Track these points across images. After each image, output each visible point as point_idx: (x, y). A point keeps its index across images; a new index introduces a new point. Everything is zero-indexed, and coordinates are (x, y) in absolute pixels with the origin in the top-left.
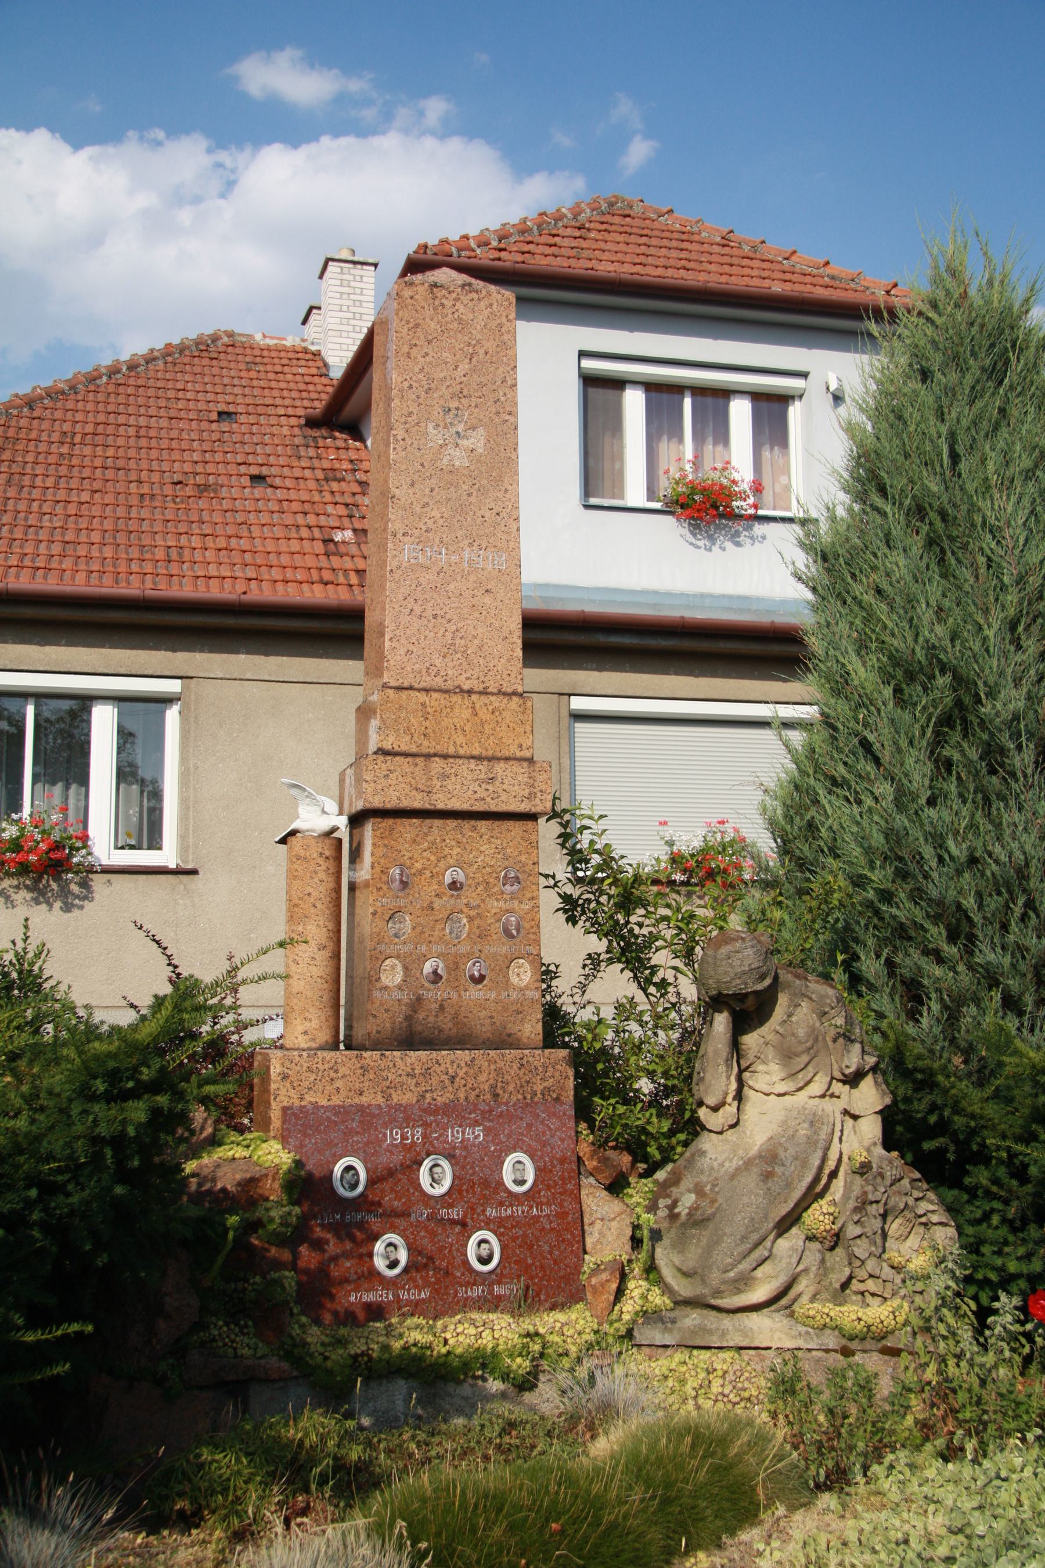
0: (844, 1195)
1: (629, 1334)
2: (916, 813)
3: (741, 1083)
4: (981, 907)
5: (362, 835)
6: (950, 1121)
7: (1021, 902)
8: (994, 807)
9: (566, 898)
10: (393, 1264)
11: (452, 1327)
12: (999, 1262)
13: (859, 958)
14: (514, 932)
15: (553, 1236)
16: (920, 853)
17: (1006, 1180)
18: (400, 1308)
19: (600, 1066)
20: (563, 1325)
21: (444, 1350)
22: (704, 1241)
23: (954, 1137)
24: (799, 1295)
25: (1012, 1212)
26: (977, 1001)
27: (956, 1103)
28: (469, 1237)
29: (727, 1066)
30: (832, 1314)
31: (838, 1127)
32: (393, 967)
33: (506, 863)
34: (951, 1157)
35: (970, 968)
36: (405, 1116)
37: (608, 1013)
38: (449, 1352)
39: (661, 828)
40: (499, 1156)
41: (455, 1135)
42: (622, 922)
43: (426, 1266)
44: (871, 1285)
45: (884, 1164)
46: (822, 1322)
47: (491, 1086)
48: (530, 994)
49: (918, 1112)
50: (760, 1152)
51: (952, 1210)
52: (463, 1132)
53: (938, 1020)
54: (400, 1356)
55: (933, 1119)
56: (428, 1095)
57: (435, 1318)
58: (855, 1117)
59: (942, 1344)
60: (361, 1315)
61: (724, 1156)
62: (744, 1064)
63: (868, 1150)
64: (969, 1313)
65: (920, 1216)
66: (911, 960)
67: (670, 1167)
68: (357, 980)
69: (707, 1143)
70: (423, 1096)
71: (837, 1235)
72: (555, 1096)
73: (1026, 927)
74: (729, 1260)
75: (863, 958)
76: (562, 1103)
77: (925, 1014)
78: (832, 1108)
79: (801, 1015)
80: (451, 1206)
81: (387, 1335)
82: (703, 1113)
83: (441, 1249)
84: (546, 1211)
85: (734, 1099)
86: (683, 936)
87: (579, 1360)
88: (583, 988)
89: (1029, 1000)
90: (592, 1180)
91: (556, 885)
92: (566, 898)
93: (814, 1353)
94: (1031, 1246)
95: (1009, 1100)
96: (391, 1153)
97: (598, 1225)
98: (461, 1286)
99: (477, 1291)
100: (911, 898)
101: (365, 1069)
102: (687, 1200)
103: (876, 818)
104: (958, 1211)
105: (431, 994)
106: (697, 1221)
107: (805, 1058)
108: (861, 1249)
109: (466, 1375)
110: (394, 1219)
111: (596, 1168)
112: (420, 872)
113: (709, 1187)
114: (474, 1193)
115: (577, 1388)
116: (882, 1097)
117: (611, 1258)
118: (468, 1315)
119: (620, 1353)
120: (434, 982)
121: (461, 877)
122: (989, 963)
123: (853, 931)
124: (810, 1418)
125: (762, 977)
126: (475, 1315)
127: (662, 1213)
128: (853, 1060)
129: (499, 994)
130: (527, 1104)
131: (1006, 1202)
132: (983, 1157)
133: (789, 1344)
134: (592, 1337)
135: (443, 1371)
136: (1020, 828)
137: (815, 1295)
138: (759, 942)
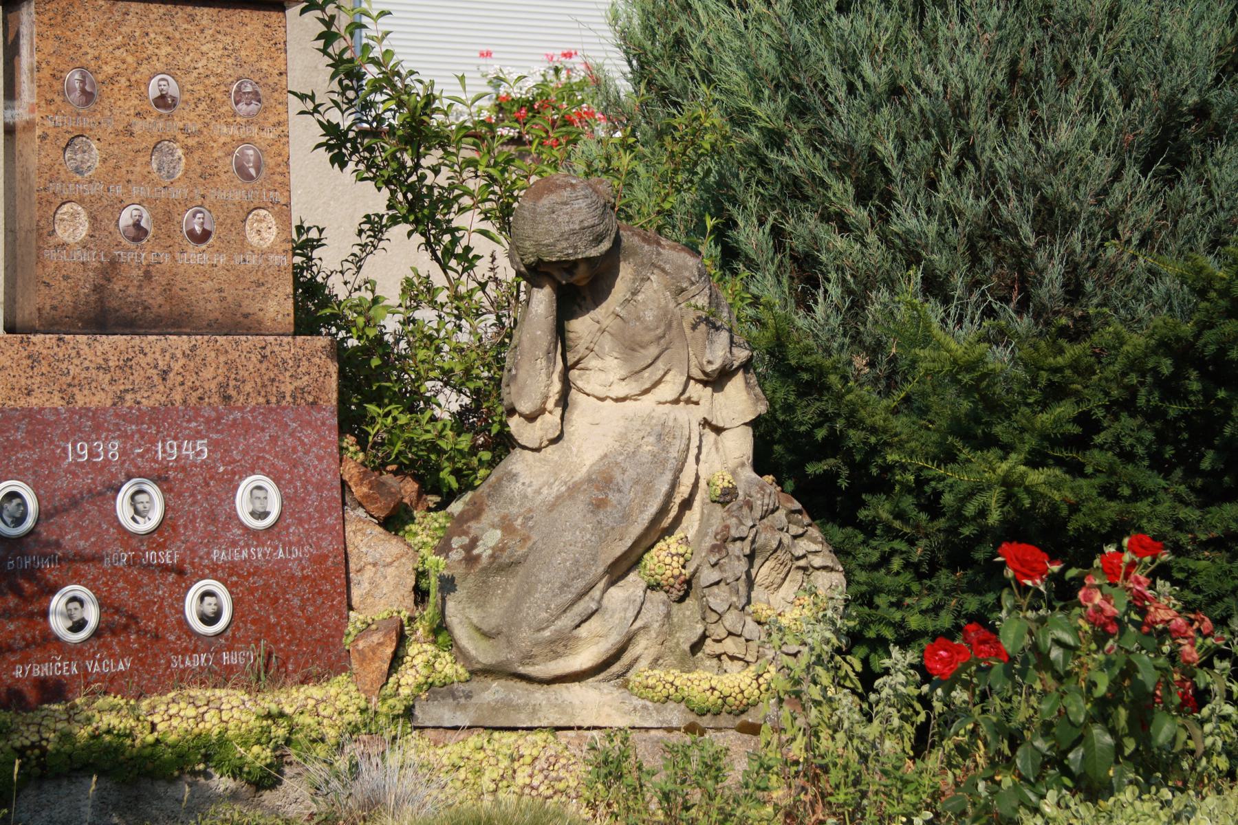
0: (699, 531)
1: (409, 713)
2: (822, 23)
3: (567, 385)
4: (901, 156)
5: (19, 21)
6: (844, 436)
7: (955, 148)
8: (929, 15)
9: (331, 129)
10: (78, 626)
11: (163, 707)
12: (897, 616)
13: (736, 224)
14: (252, 171)
15: (306, 586)
16: (824, 79)
17: (912, 512)
18: (87, 685)
19: (375, 362)
20: (318, 702)
21: (150, 739)
22: (512, 591)
23: (848, 455)
24: (636, 660)
25: (917, 553)
26: (891, 284)
27: (853, 412)
28: (188, 588)
29: (549, 360)
30: (677, 683)
31: (695, 442)
32: (74, 215)
33: (240, 72)
34: (843, 484)
35: (884, 238)
36: (94, 423)
37: (391, 293)
38: (157, 741)
39: (482, 61)
40: (231, 481)
41: (168, 451)
42: (409, 164)
43: (126, 627)
44: (730, 646)
45: (754, 491)
46: (665, 693)
47: (220, 385)
48: (276, 259)
49: (801, 424)
50: (589, 474)
51: (839, 551)
52: (179, 447)
53: (838, 309)
54: (88, 747)
55: (821, 434)
56: (129, 397)
57: (139, 697)
58: (718, 430)
59: (814, 712)
60: (31, 695)
61: (541, 480)
62: (571, 358)
63: (734, 473)
64: (852, 675)
65: (798, 558)
66: (806, 227)
67: (468, 496)
68: (21, 235)
69: (518, 462)
70: (121, 398)
71: (689, 582)
72: (311, 399)
73: (961, 184)
74: (544, 615)
75: (741, 224)
76: (320, 409)
77: (820, 300)
78: (689, 417)
79: (650, 293)
80: (162, 547)
81: (68, 720)
82: (514, 424)
83: (148, 605)
84: (297, 553)
85: (556, 405)
86: (497, 189)
87: (340, 747)
88: (358, 263)
89: (958, 281)
90: (361, 512)
91: (316, 110)
92: (331, 129)
93: (653, 732)
94: (939, 595)
95: (923, 412)
96: (74, 474)
97: (369, 572)
98: (176, 654)
99: (199, 660)
100: (810, 143)
101: (34, 360)
102: (491, 539)
103: (766, 28)
104: (848, 554)
105: (130, 256)
106: (503, 565)
107: (653, 351)
108: (719, 598)
109: (181, 769)
110: (77, 564)
111: (366, 496)
112: (112, 80)
113: (520, 521)
114: (195, 530)
115: (335, 783)
116: (755, 404)
117: (385, 615)
118: (185, 692)
119: (394, 738)
120: (136, 239)
121: (173, 89)
122: (909, 232)
123: (730, 187)
124: (640, 806)
125: (598, 239)
126: (195, 692)
127: (457, 555)
128: (718, 353)
129: (231, 258)
130: (271, 410)
131: (912, 542)
132: (883, 485)
133: (620, 721)
134: (357, 718)
135: (150, 766)
136: (961, 45)
137: (656, 660)
138: (595, 191)
